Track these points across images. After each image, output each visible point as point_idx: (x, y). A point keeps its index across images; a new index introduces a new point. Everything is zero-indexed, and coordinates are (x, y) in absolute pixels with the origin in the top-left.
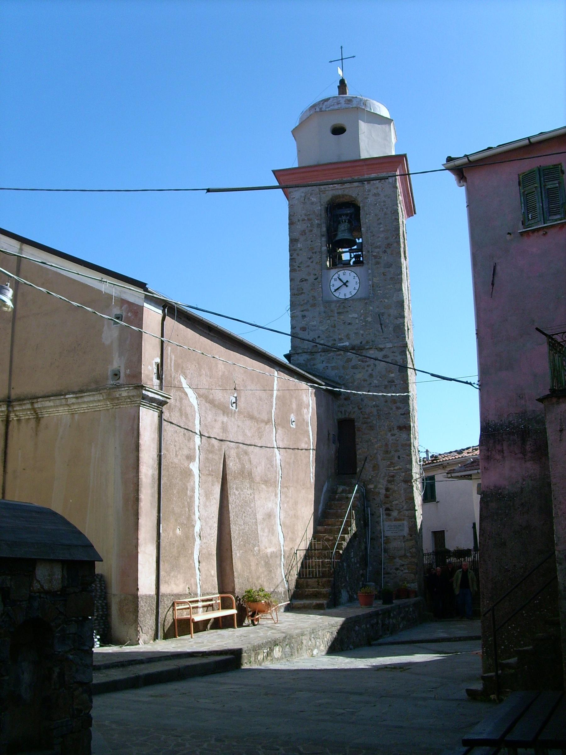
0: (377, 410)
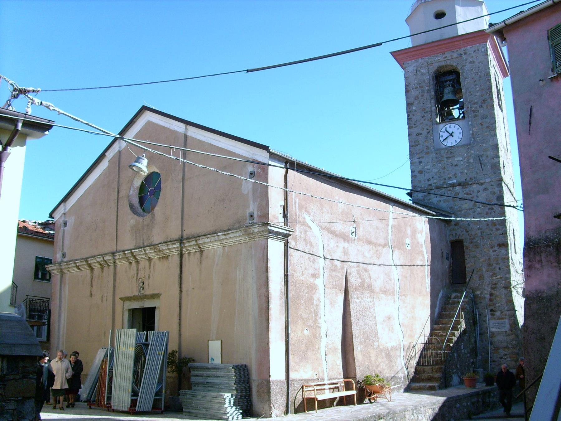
0: (481, 232)
